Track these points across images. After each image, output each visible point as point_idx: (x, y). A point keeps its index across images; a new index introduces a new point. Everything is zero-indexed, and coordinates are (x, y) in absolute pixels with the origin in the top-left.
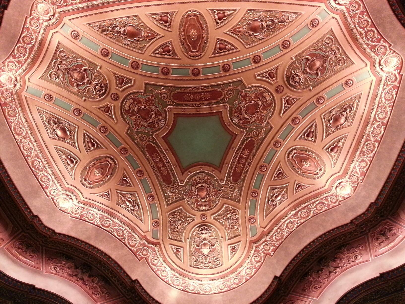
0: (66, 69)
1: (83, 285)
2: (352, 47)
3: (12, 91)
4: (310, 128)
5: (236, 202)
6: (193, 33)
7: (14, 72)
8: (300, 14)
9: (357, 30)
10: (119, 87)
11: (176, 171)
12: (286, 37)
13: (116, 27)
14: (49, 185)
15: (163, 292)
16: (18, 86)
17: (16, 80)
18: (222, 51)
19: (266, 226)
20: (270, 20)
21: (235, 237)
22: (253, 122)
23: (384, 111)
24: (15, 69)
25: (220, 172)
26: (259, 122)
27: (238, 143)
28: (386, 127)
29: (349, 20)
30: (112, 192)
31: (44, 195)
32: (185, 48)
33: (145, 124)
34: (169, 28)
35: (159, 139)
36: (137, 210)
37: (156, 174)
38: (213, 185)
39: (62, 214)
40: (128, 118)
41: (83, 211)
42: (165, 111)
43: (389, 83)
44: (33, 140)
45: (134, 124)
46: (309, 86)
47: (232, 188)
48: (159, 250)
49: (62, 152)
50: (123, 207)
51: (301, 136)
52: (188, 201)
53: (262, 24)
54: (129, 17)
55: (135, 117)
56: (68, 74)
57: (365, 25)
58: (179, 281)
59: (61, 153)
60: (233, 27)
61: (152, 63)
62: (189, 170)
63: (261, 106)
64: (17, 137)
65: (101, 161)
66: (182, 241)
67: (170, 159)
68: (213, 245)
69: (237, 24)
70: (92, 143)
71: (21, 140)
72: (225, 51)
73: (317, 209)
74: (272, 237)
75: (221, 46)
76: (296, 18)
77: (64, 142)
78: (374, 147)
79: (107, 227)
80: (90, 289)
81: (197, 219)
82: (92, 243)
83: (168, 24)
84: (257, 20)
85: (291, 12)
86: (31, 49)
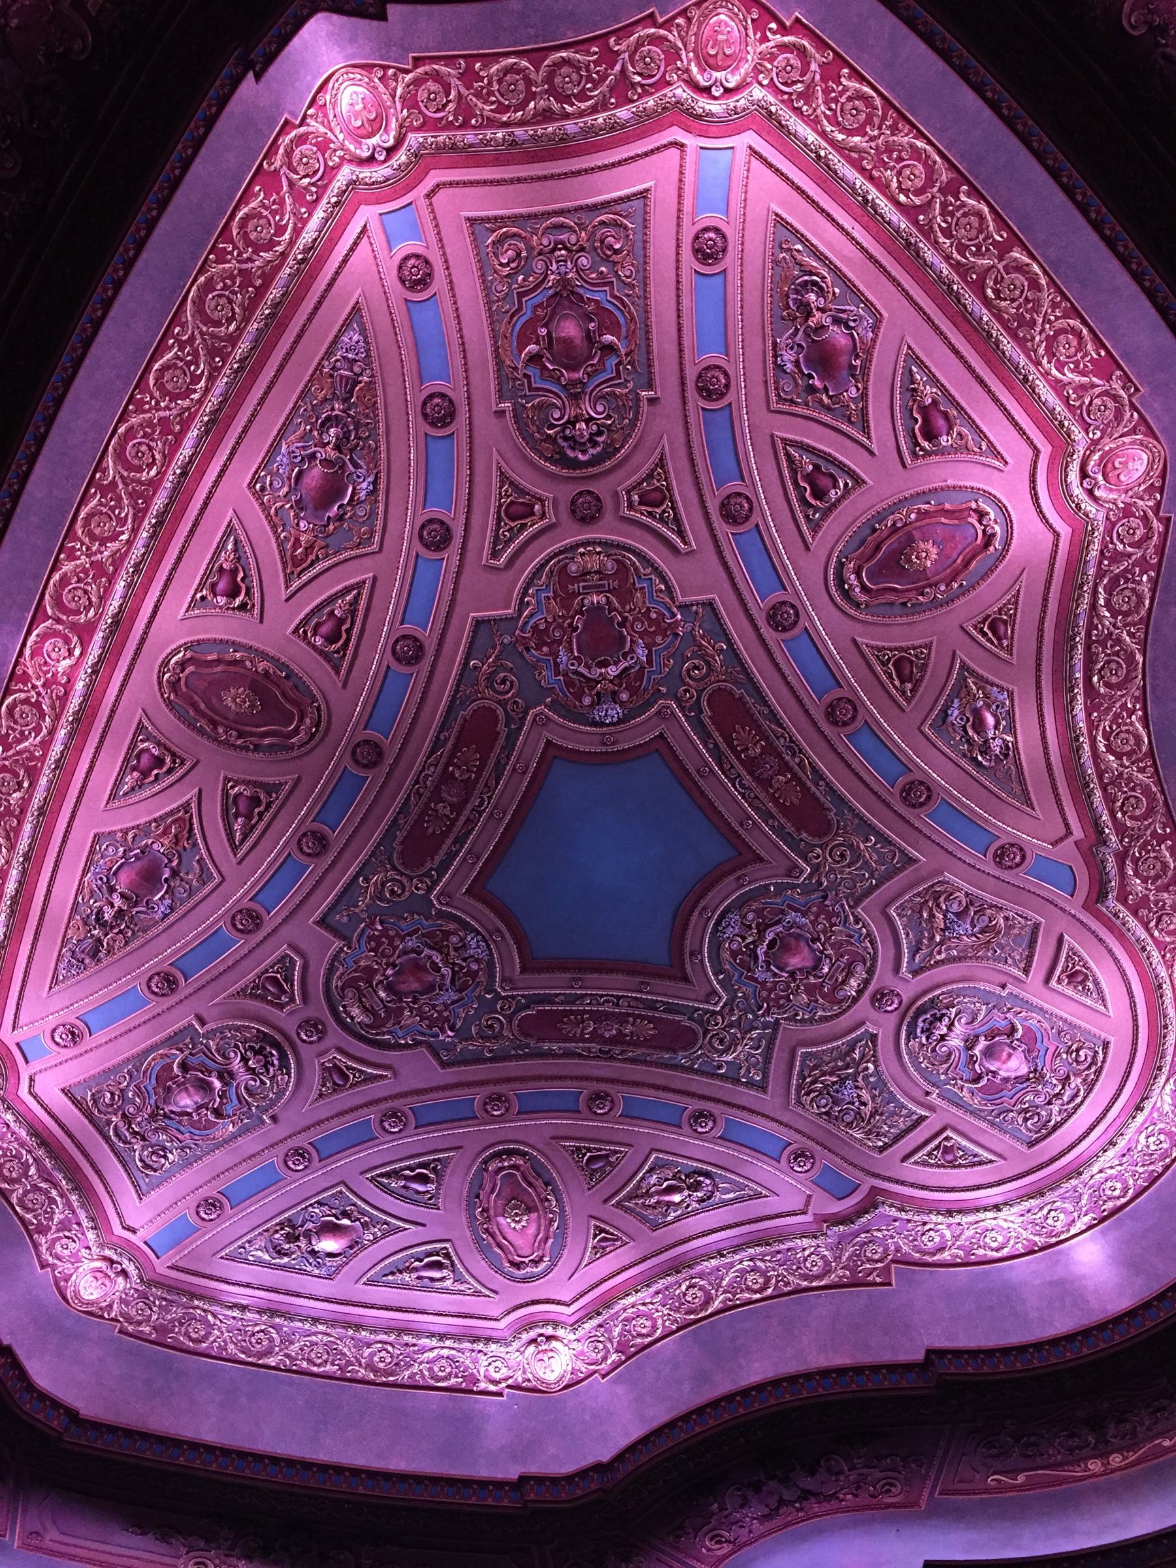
0: (153, 1116)
1: (826, 1506)
2: (579, 173)
3: (136, 1290)
4: (794, 472)
5: (901, 870)
6: (235, 699)
8: (356, 309)
9: (522, 123)
10: (287, 1004)
11: (662, 993)
12: (414, 399)
13: (100, 911)
14: (467, 1368)
15: (1050, 1283)
16: (131, 1269)
17: (112, 1262)
18: (344, 636)
19: (1067, 825)
20: (323, 425)
22: (649, 656)
23: (900, 159)
25: (760, 859)
26: (665, 636)
27: (695, 748)
28: (970, 184)
29: (470, 137)
30: (605, 1217)
31: (485, 1402)
32: (270, 746)
34: (182, 763)
35: (521, 985)
36: (715, 1186)
37: (633, 1061)
38: (790, 907)
39: (577, 1393)
40: (400, 1033)
41: (610, 1331)
42: (441, 914)
43: (799, 87)
45: (430, 1027)
46: (638, 399)
47: (842, 856)
48: (897, 1203)
49: (392, 1273)
50: (678, 1219)
51: (807, 517)
52: (793, 1019)
53: (326, 462)
54: (89, 861)
55: (407, 1013)
56: (170, 1118)
57: (521, 86)
58: (1060, 1212)
59: (390, 1278)
60: (284, 564)
61: (275, 859)
62: (687, 950)
63: (608, 602)
64: (272, 1361)
65: (488, 1188)
66: (922, 1119)
68: (1013, 1029)
69: (280, 544)
71: (287, 1356)
72: (347, 626)
73: (1126, 614)
74: (1121, 830)
75: (324, 630)
76: (363, 331)
77: (364, 1248)
78: (1020, 268)
79: (708, 1300)
80: (856, 1496)
81: (876, 1023)
82: (723, 1386)
83: (168, 760)
84: (300, 473)
85: (337, 338)
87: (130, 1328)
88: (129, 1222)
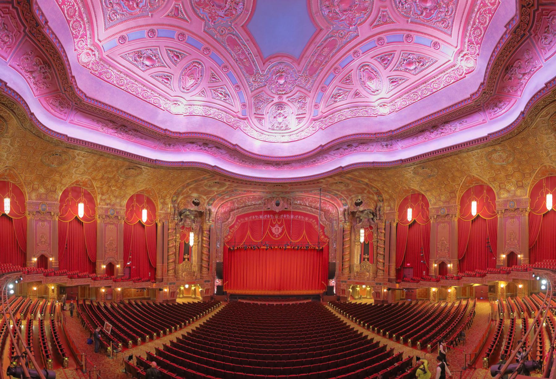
2: (460, 25)
7: (85, 47)
16: (97, 53)
17: (92, 51)
21: (302, 114)
22: (343, 20)
24: (84, 44)
27: (321, 38)
33: (221, 13)
44: (133, 81)
64: (123, 88)
67: (251, 50)
68: (286, 117)
70: (177, 56)
77: (155, 67)
78: (417, 99)
86: (81, 15)
87: (93, 72)
88: (100, 38)
